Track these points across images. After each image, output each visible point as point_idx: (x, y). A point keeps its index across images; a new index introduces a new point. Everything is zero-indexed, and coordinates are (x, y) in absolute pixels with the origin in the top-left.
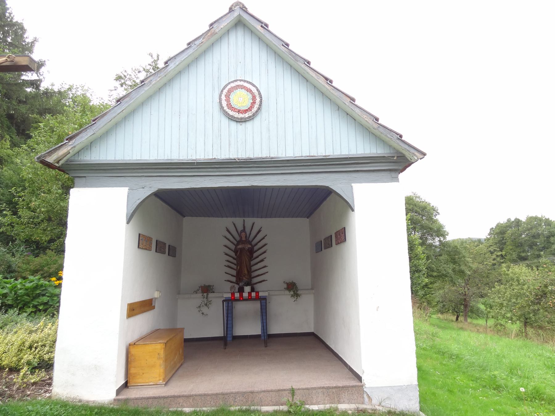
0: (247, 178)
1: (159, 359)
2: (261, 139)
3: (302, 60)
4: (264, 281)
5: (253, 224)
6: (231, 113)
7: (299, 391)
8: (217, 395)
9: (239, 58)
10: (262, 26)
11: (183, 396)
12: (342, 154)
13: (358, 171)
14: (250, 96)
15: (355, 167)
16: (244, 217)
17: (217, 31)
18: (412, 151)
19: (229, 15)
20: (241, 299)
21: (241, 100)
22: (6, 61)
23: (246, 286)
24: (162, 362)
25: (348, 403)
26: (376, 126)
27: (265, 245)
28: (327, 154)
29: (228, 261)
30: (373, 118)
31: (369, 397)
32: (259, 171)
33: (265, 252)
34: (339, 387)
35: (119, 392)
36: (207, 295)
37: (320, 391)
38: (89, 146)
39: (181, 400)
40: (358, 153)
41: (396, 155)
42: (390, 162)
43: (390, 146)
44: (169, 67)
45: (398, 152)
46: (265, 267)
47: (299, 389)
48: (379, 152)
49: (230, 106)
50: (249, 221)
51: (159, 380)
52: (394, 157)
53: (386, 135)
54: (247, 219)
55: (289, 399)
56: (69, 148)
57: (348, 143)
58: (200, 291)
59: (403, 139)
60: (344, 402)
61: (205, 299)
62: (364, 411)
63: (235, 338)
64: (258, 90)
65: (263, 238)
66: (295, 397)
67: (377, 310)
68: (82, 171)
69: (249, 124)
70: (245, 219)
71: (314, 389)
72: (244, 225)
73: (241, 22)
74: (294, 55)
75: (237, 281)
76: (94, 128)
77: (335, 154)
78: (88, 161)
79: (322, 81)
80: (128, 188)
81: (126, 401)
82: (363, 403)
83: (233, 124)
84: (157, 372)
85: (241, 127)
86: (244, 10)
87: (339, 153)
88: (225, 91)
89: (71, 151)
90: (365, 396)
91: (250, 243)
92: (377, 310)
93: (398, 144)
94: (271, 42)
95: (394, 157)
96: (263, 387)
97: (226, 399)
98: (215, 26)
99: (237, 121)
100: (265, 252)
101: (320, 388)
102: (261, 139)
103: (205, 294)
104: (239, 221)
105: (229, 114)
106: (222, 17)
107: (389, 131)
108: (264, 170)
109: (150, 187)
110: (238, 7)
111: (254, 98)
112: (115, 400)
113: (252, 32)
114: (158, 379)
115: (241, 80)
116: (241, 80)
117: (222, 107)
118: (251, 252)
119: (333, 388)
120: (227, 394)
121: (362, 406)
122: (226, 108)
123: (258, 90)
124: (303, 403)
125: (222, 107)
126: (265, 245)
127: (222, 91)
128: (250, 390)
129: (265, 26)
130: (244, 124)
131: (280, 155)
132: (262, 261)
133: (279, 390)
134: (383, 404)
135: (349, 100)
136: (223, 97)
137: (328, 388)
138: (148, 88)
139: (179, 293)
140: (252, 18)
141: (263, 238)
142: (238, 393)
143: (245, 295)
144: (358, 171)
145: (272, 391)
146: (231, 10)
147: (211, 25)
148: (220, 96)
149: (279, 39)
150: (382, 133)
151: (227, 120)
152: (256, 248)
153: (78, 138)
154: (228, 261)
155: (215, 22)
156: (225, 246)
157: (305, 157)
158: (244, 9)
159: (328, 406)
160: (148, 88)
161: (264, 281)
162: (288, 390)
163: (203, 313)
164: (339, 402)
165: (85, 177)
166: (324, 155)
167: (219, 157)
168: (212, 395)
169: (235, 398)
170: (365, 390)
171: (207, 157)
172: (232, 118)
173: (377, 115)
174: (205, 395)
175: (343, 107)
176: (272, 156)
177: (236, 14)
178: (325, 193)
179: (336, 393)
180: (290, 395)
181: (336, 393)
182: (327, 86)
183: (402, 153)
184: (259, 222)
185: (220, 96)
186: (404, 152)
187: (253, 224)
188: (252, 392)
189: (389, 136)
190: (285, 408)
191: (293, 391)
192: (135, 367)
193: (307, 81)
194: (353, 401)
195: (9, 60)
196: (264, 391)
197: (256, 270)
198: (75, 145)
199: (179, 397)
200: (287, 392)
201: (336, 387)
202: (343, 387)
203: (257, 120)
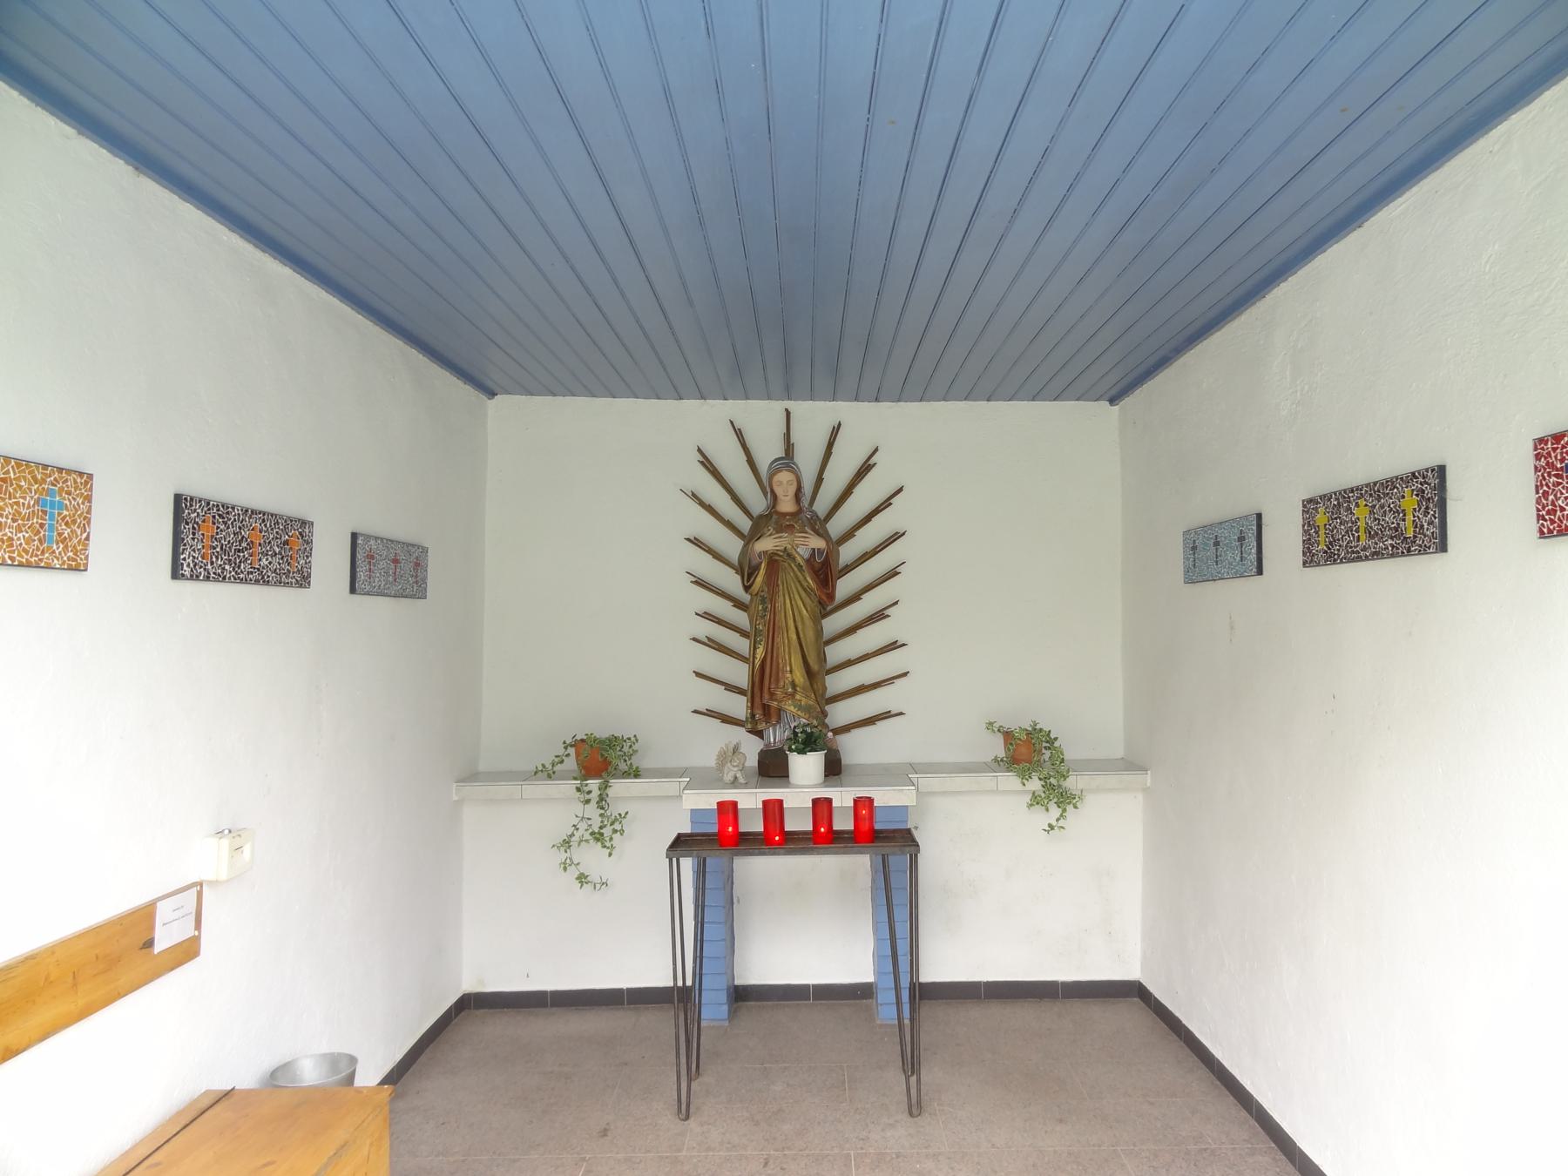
4: (887, 715)
5: (835, 431)
27: (896, 537)
29: (707, 616)
36: (605, 787)
46: (893, 646)
50: (813, 418)
54: (800, 408)
58: (571, 763)
61: (592, 811)
65: (886, 504)
100: (893, 574)
103: (594, 784)
104: (762, 419)
126: (896, 537)
132: (878, 616)
139: (472, 776)
141: (886, 504)
154: (707, 616)
156: (696, 542)
161: (887, 715)
184: (867, 423)
187: (835, 431)
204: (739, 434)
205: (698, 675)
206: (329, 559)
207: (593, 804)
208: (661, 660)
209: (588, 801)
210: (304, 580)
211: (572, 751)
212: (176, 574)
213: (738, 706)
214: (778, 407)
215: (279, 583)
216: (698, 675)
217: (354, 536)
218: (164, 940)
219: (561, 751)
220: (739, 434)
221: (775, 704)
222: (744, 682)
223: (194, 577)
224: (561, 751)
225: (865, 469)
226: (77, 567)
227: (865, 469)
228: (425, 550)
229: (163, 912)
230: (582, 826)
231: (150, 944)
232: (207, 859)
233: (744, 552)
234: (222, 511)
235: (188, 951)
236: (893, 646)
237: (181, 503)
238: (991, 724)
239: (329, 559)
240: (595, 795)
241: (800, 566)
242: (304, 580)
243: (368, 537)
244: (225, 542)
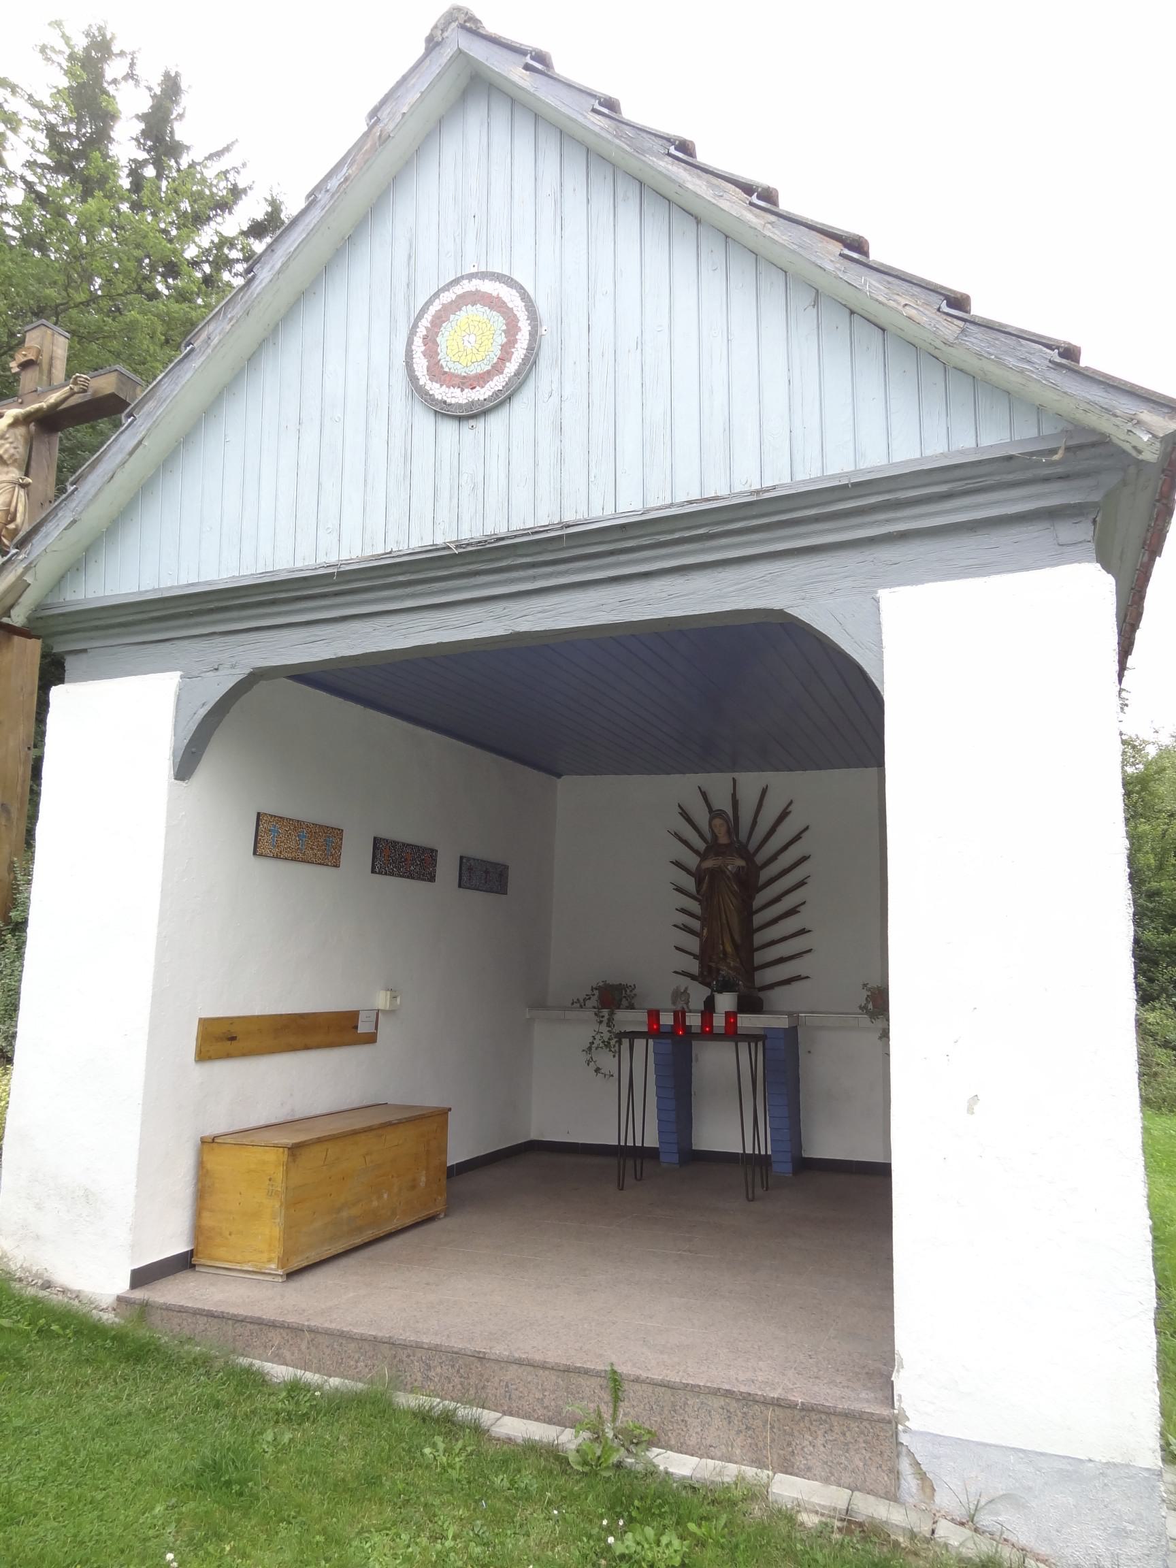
0: (498, 608)
1: (270, 1194)
2: (536, 464)
3: (657, 145)
4: (798, 978)
5: (764, 792)
6: (439, 391)
7: (637, 1387)
8: (375, 1341)
9: (493, 205)
10: (527, 67)
11: (283, 1326)
12: (830, 472)
13: (903, 536)
14: (500, 322)
15: (888, 521)
16: (733, 769)
17: (391, 126)
18: (1125, 406)
19: (427, 61)
20: (708, 1033)
21: (471, 341)
22: (72, 394)
23: (720, 992)
24: (277, 1205)
25: (826, 1481)
26: (950, 329)
27: (804, 859)
28: (768, 483)
29: (683, 911)
30: (935, 299)
31: (922, 1476)
32: (534, 578)
33: (802, 883)
34: (792, 1406)
35: (141, 1277)
36: (612, 1014)
37: (717, 1403)
38: (80, 563)
39: (276, 1337)
40: (898, 457)
41: (1062, 444)
42: (1046, 480)
43: (1040, 410)
44: (257, 282)
45: (1077, 428)
46: (803, 932)
47: (637, 1380)
48: (986, 441)
49: (437, 372)
50: (750, 783)
51: (270, 1261)
52: (1053, 451)
53: (999, 362)
54: (742, 777)
55: (603, 1408)
56: (20, 570)
57: (870, 427)
58: (594, 1002)
59: (1084, 362)
60: (805, 1473)
61: (604, 1028)
62: (871, 1531)
63: (808, 1167)
64: (525, 296)
65: (798, 837)
66: (624, 1407)
67: (970, 1110)
68: (75, 636)
69: (496, 422)
70: (736, 775)
71: (695, 1390)
72: (734, 795)
73: (473, 78)
74: (630, 132)
75: (701, 973)
76: (74, 504)
77: (800, 477)
78: (78, 602)
79: (733, 204)
80: (179, 673)
81: (145, 1308)
82: (892, 1497)
83: (449, 428)
84: (263, 1239)
85: (471, 434)
86: (470, 30)
87: (815, 473)
88: (425, 322)
89: (28, 579)
90: (905, 1466)
91: (749, 857)
92: (970, 1110)
93: (1055, 388)
94: (556, 109)
95: (1053, 451)
96: (530, 1346)
97: (401, 1361)
98: (384, 114)
99: (460, 419)
100: (802, 883)
101: (716, 1392)
102: (536, 464)
103: (605, 1012)
104: (718, 784)
105: (432, 397)
106: (405, 79)
107: (1011, 341)
108: (551, 575)
109: (233, 667)
110: (454, 25)
111: (512, 329)
112: (120, 1299)
113: (516, 102)
114: (265, 1256)
115: (471, 276)
116: (471, 276)
117: (413, 378)
118: (748, 883)
119: (767, 1403)
120: (405, 1347)
121: (872, 1508)
122: (424, 380)
123: (525, 296)
124: (635, 1440)
125: (413, 378)
126: (804, 859)
127: (415, 326)
128: (479, 1346)
129: (539, 63)
130: (480, 424)
131: (596, 513)
132: (793, 911)
133: (568, 1370)
134: (985, 1520)
135: (837, 248)
136: (418, 346)
137: (747, 1399)
138: (203, 358)
139: (539, 1004)
140: (495, 48)
141: (798, 837)
142: (436, 1349)
143: (719, 1021)
144: (903, 536)
145: (544, 1366)
146: (433, 44)
147: (374, 113)
148: (410, 342)
149: (580, 90)
150: (979, 356)
151: (432, 417)
152: (765, 875)
153: (37, 539)
154: (683, 911)
155: (383, 102)
156: (677, 864)
157: (682, 505)
158: (471, 26)
159: (731, 1471)
160: (203, 358)
161: (798, 978)
162: (597, 1374)
163: (597, 1070)
164: (787, 1467)
165: (85, 651)
166: (757, 487)
167: (404, 547)
168: (363, 1339)
169: (429, 1368)
170: (904, 1439)
171: (369, 552)
172: (443, 412)
173: (957, 285)
174: (342, 1335)
175: (836, 283)
176: (569, 517)
177: (447, 52)
178: (780, 634)
179: (781, 1427)
180: (607, 1397)
181: (781, 1427)
182: (750, 217)
183: (1093, 431)
184: (784, 785)
185: (410, 342)
186: (1105, 425)
187: (764, 792)
188: (481, 1358)
189: (1011, 361)
190: (568, 1439)
191: (615, 1383)
192: (212, 1211)
193: (698, 221)
194: (847, 1478)
195: (76, 389)
196: (519, 1363)
197: (773, 943)
198: (32, 557)
199: (273, 1325)
200: (595, 1382)
201: (777, 1403)
202: (807, 1409)
203: (521, 406)
204: (704, 795)
205: (677, 948)
206: (447, 868)
207: (604, 1024)
208: (652, 942)
209: (601, 1022)
210: (432, 879)
211: (596, 992)
212: (373, 871)
213: (694, 967)
214: (728, 776)
215: (419, 879)
216: (677, 948)
217: (461, 858)
218: (363, 1028)
219: (590, 992)
220: (704, 795)
221: (713, 965)
222: (696, 950)
223: (380, 873)
224: (590, 992)
225: (784, 814)
226: (337, 866)
227: (784, 814)
228: (506, 867)
229: (362, 1017)
230: (598, 1037)
231: (356, 1027)
232: (382, 1000)
233: (699, 866)
234: (394, 844)
235: (371, 1039)
236: (803, 932)
237: (376, 841)
238: (865, 985)
239: (447, 868)
240: (605, 1019)
241: (728, 878)
242: (432, 879)
243: (469, 859)
244: (399, 859)
